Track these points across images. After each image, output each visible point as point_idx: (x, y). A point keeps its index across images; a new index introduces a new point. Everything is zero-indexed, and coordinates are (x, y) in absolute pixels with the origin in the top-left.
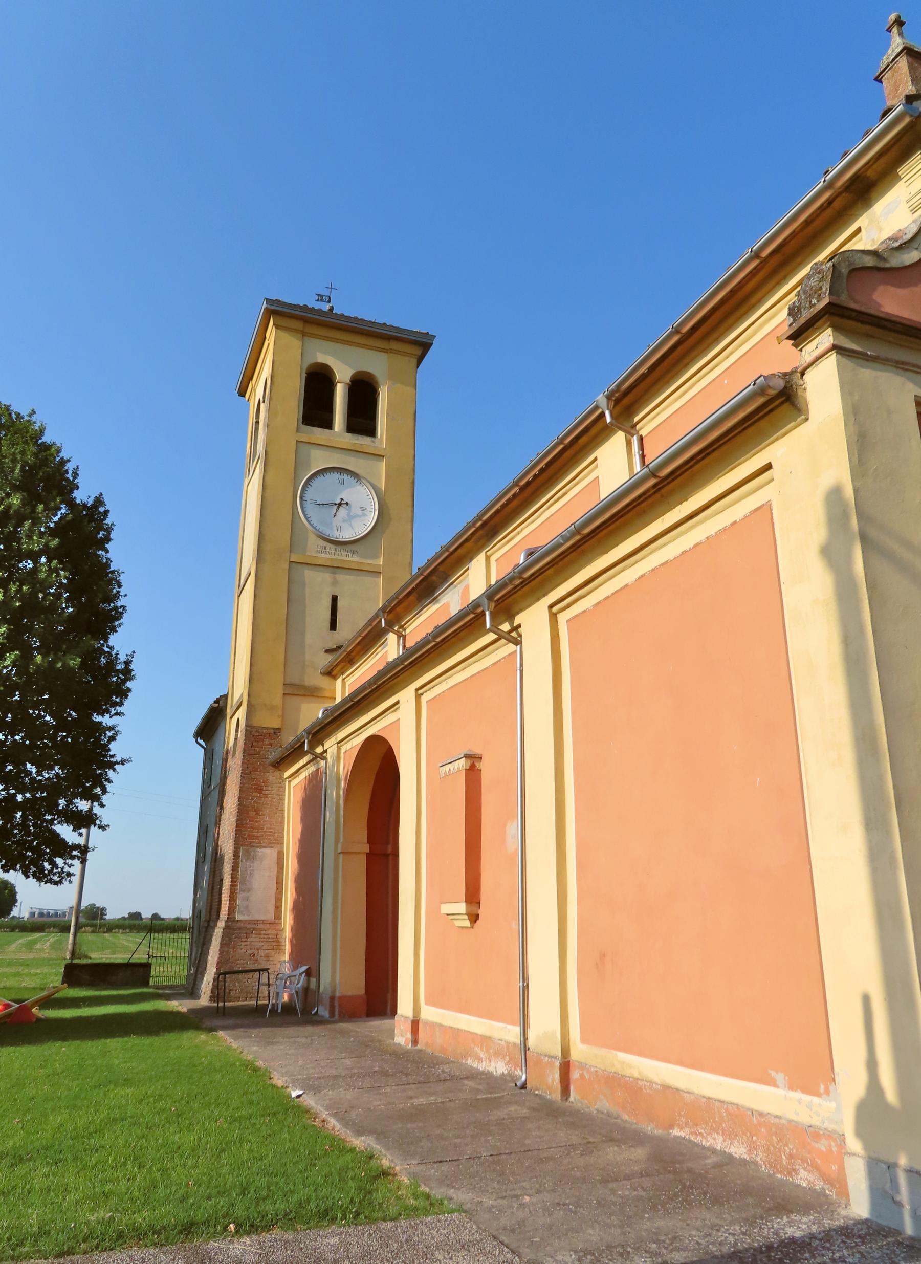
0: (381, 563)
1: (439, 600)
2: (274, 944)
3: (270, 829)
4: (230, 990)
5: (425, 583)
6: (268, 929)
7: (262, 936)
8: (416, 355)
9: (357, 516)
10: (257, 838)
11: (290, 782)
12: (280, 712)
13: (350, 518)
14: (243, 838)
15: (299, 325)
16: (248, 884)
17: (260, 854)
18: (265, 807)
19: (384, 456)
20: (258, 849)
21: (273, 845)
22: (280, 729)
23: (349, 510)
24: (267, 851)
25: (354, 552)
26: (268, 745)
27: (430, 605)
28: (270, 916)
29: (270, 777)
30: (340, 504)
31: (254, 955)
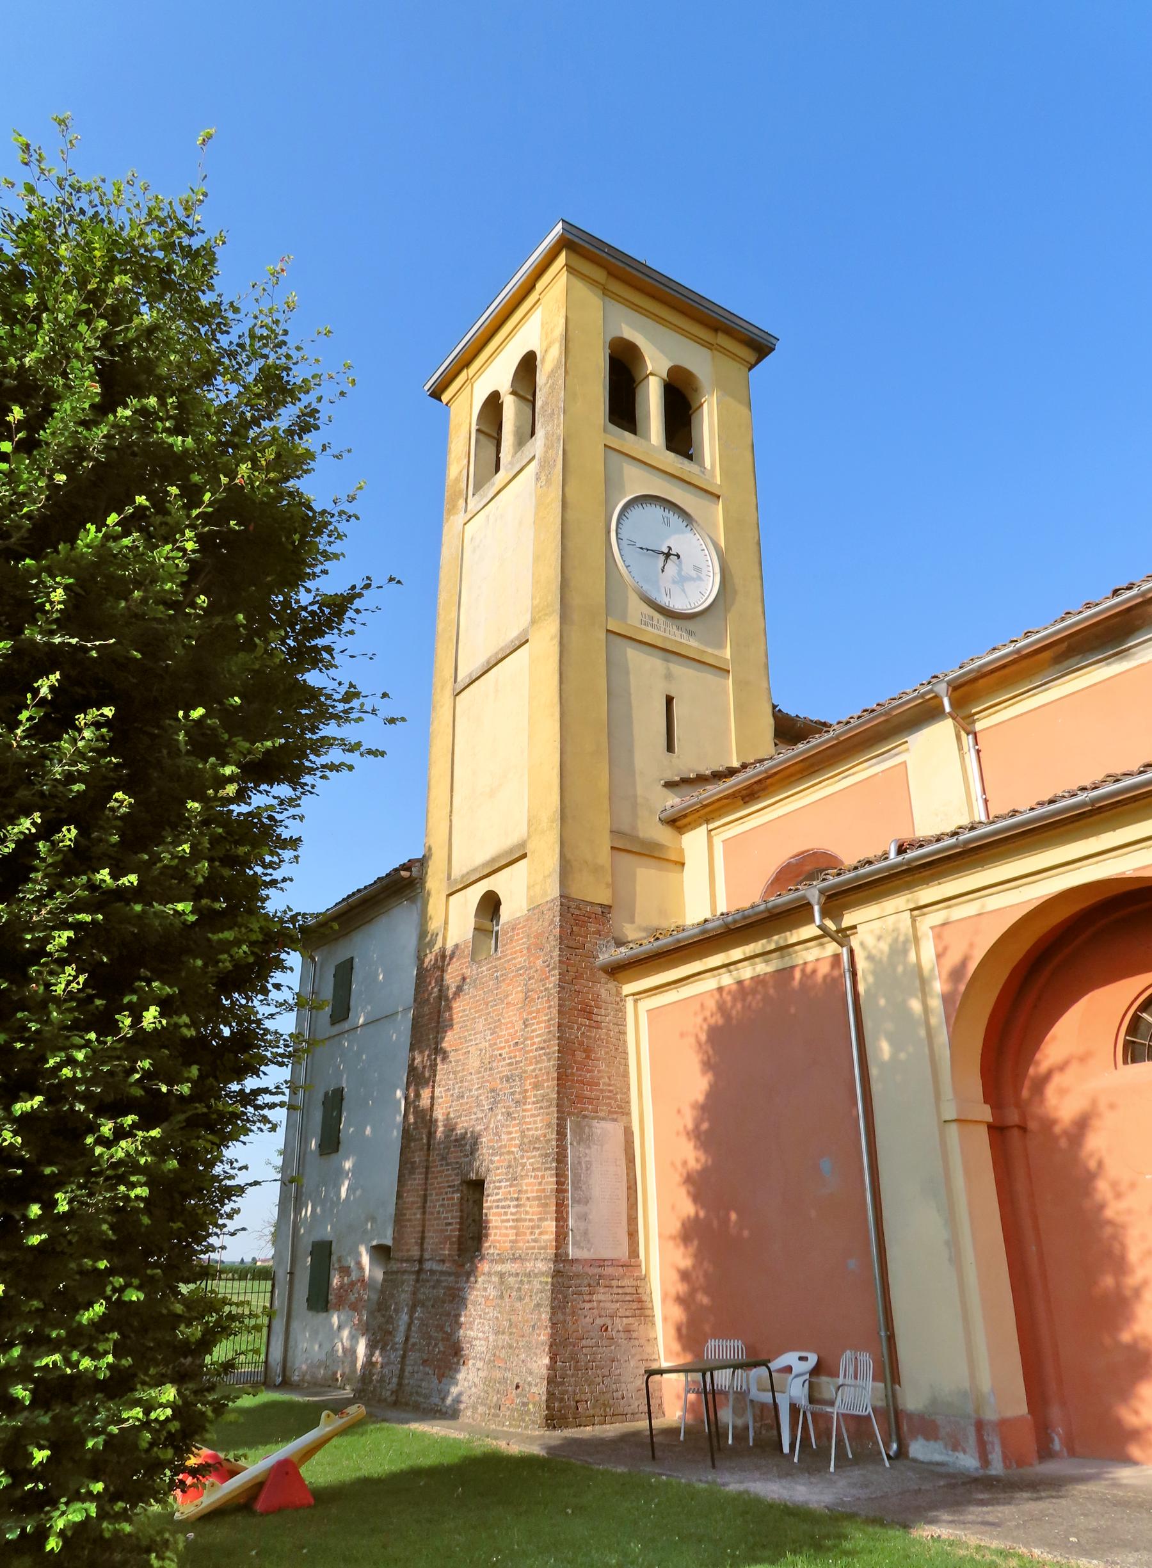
0: (728, 656)
1: (1135, 654)
2: (635, 1305)
3: (609, 1085)
4: (577, 1402)
5: (1118, 619)
6: (623, 1277)
7: (615, 1290)
8: (747, 362)
9: (690, 579)
10: (591, 1100)
11: (636, 1001)
12: (610, 880)
13: (682, 580)
14: (569, 1100)
15: (599, 275)
16: (584, 1188)
17: (599, 1131)
18: (599, 1046)
19: (718, 497)
20: (595, 1123)
21: (615, 1116)
22: (610, 907)
23: (680, 566)
24: (608, 1126)
25: (690, 633)
26: (594, 933)
27: (1093, 667)
28: (622, 1253)
29: (603, 990)
30: (668, 555)
31: (606, 1330)
